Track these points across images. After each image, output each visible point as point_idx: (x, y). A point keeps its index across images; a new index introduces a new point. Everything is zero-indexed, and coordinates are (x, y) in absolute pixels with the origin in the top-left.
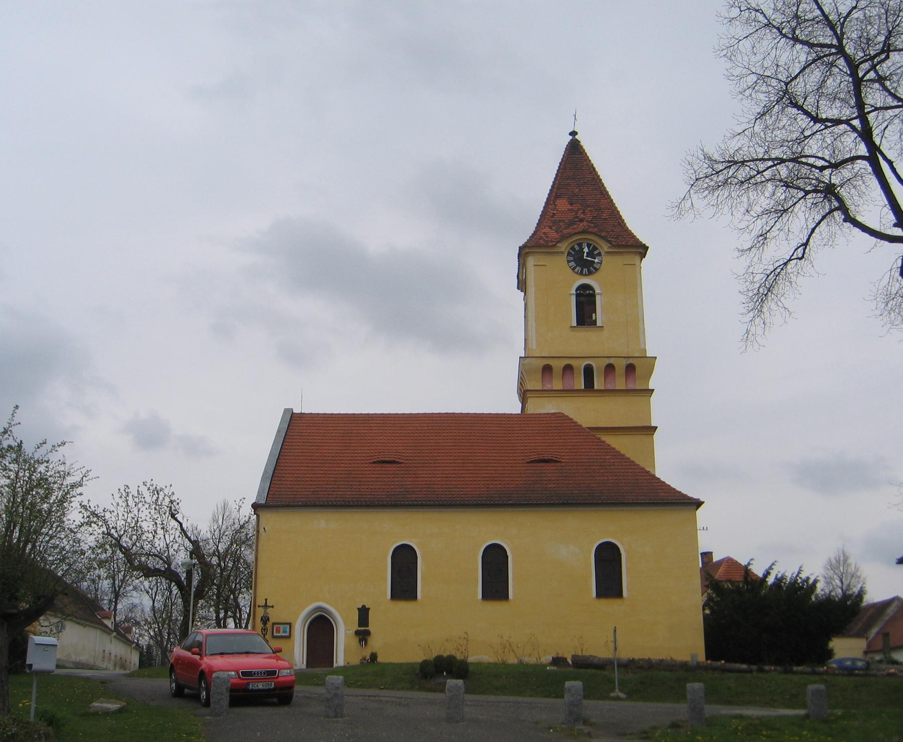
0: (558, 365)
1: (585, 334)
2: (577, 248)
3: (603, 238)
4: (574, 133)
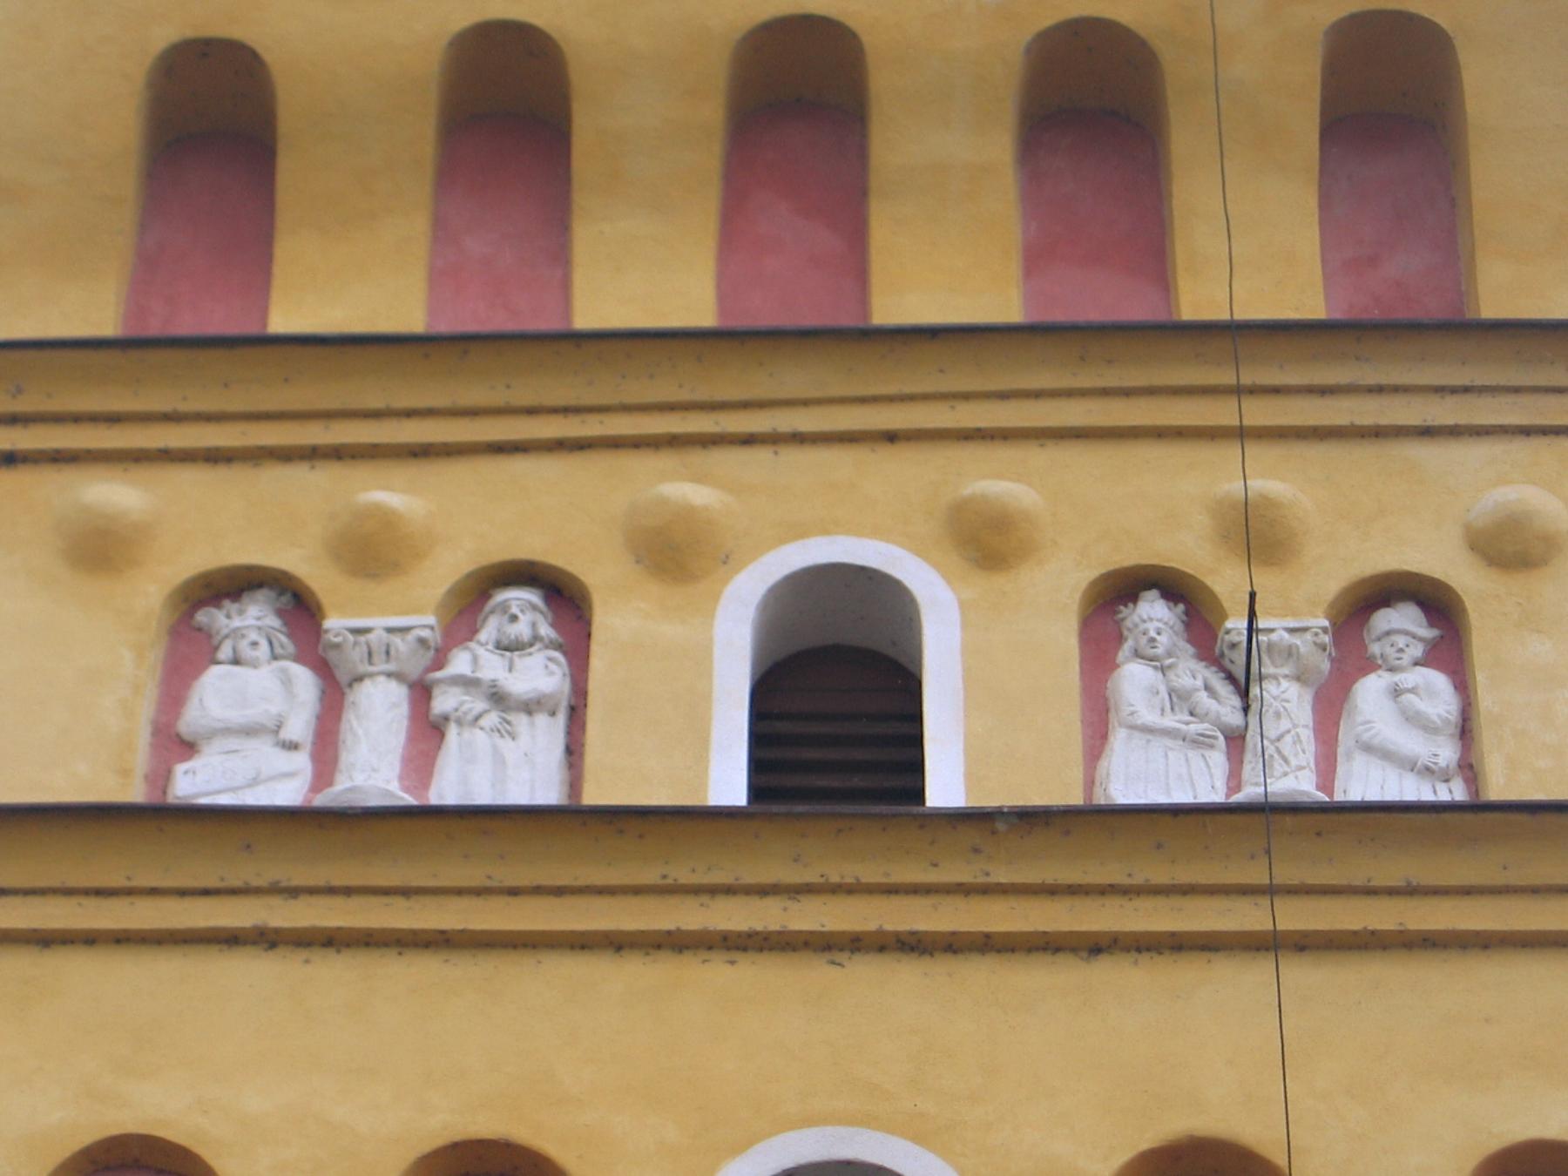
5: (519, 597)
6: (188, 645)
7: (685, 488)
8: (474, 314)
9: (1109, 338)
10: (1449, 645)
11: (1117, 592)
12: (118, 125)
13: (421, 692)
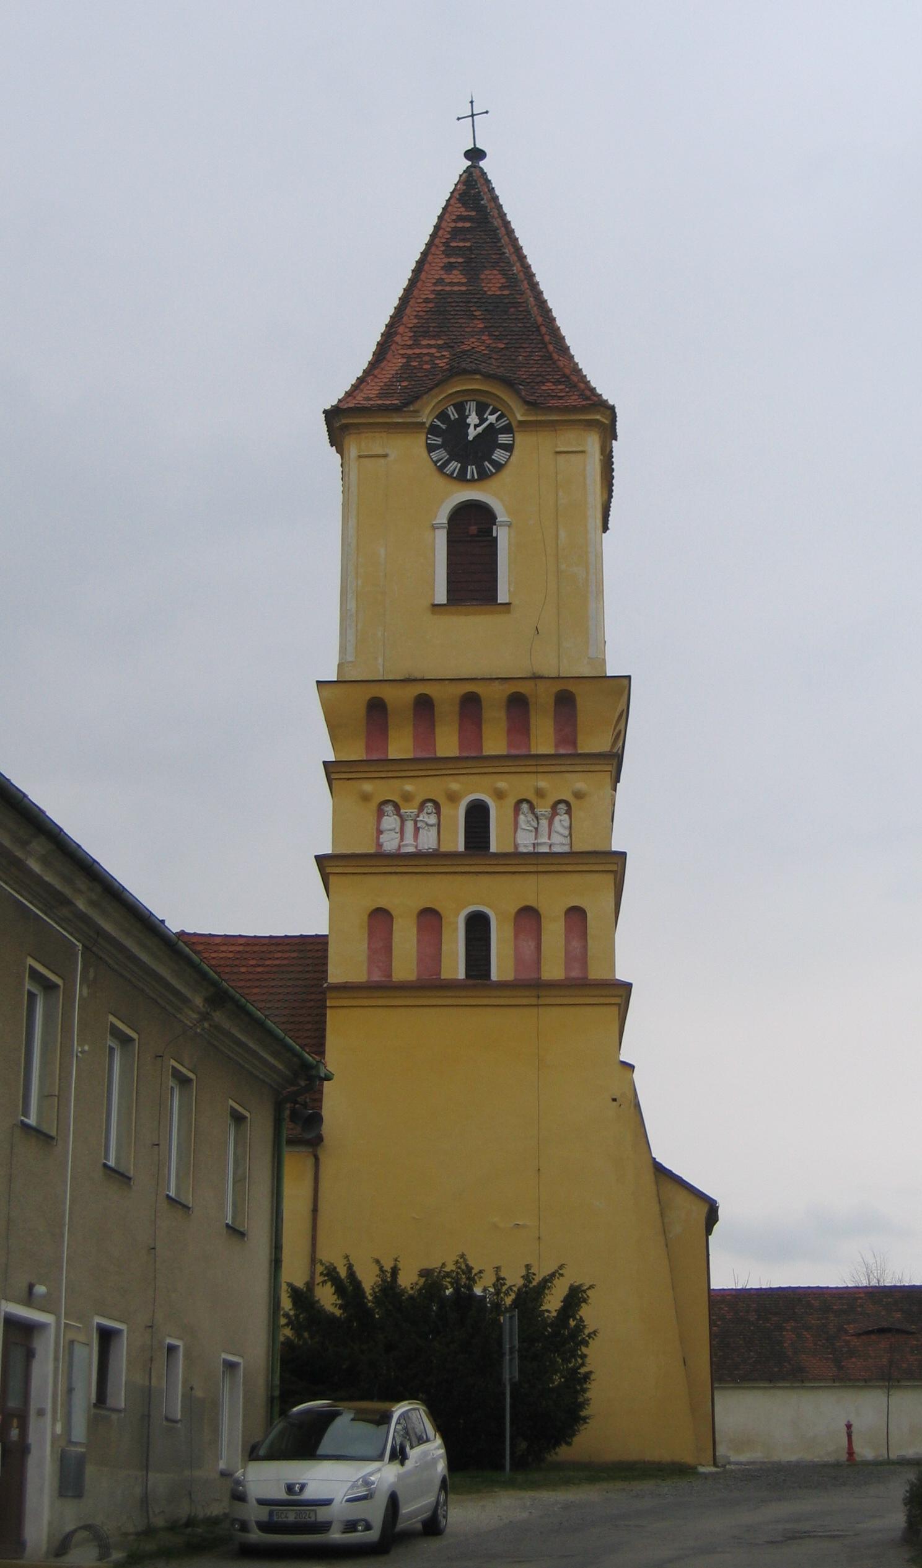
0: (400, 698)
1: (473, 626)
2: (453, 415)
3: (509, 384)
4: (475, 155)
5: (429, 804)
6: (380, 814)
7: (455, 786)
8: (419, 755)
9: (521, 760)
10: (569, 812)
11: (521, 801)
12: (362, 711)
13: (416, 822)
